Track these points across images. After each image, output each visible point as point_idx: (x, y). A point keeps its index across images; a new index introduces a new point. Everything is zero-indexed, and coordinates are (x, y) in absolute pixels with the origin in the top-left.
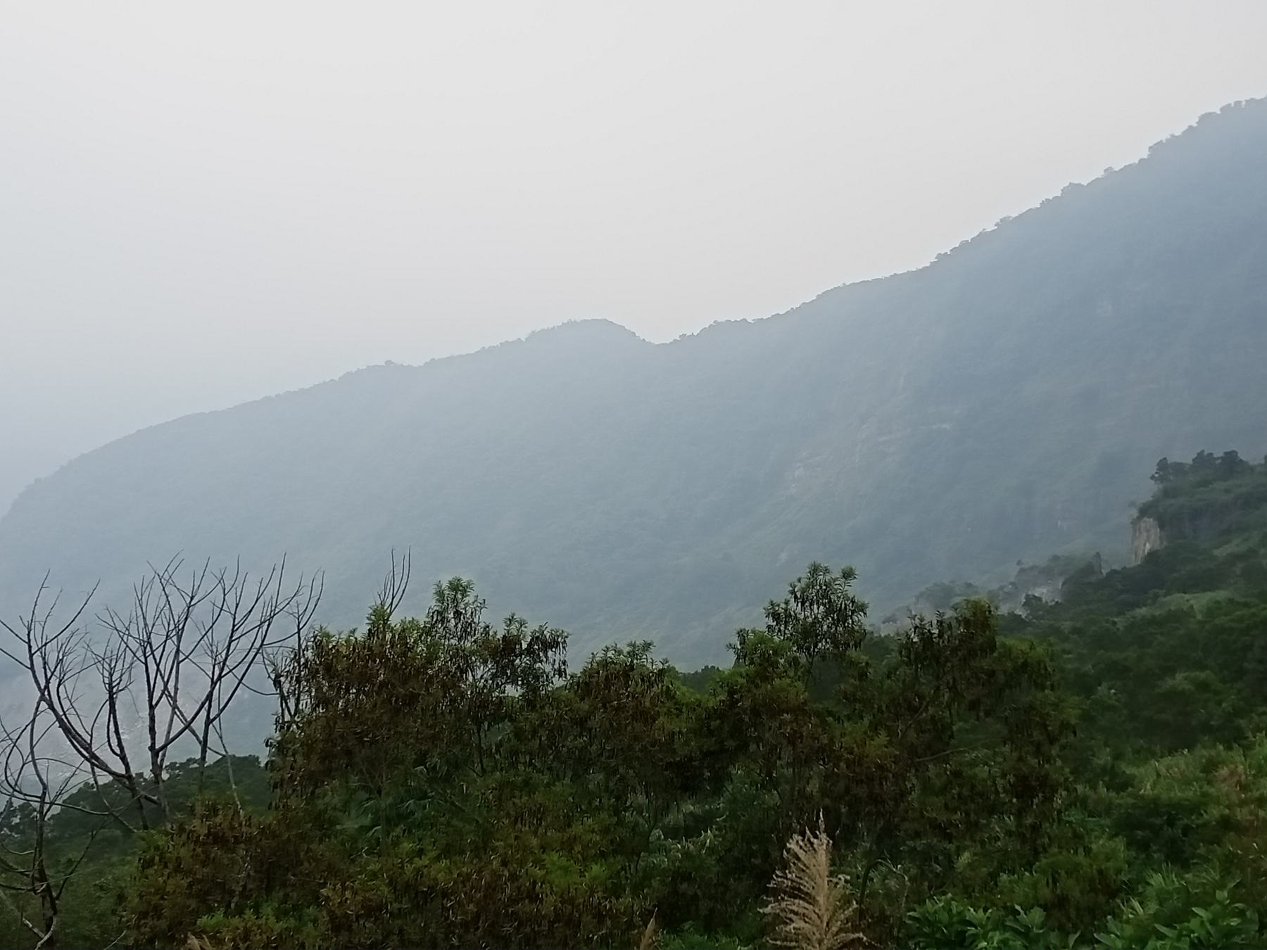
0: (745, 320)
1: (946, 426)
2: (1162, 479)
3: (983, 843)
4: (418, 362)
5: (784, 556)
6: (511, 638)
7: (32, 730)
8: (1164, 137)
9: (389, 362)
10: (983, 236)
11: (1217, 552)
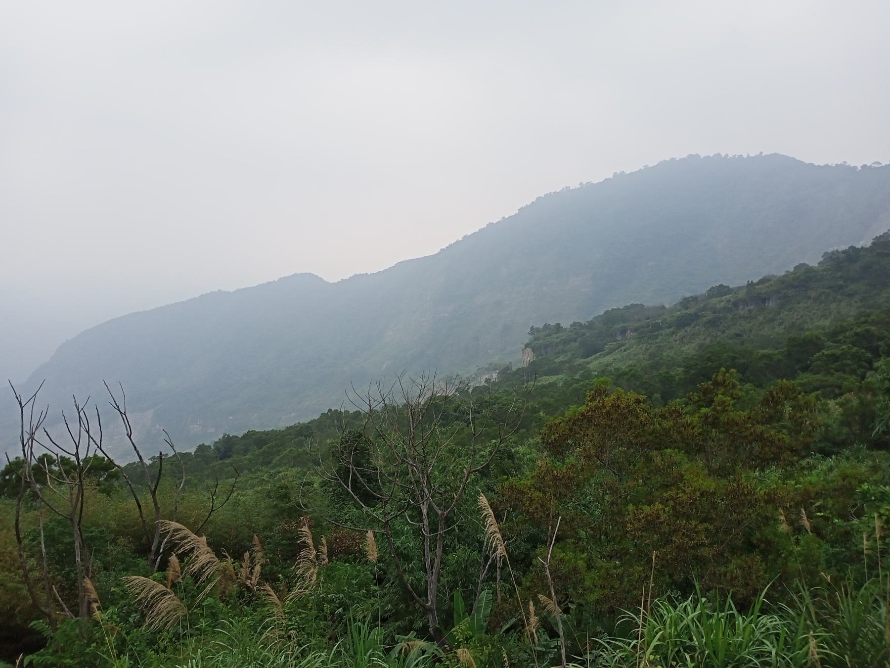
0: (367, 274)
1: (446, 315)
2: (532, 334)
3: (425, 457)
4: (232, 290)
5: (385, 366)
6: (455, 633)
7: (76, 443)
8: (524, 205)
9: (219, 290)
10: (458, 242)
11: (556, 360)
